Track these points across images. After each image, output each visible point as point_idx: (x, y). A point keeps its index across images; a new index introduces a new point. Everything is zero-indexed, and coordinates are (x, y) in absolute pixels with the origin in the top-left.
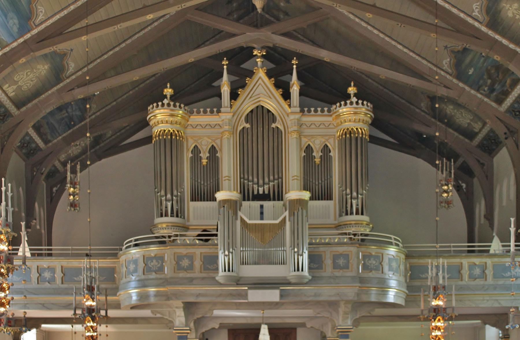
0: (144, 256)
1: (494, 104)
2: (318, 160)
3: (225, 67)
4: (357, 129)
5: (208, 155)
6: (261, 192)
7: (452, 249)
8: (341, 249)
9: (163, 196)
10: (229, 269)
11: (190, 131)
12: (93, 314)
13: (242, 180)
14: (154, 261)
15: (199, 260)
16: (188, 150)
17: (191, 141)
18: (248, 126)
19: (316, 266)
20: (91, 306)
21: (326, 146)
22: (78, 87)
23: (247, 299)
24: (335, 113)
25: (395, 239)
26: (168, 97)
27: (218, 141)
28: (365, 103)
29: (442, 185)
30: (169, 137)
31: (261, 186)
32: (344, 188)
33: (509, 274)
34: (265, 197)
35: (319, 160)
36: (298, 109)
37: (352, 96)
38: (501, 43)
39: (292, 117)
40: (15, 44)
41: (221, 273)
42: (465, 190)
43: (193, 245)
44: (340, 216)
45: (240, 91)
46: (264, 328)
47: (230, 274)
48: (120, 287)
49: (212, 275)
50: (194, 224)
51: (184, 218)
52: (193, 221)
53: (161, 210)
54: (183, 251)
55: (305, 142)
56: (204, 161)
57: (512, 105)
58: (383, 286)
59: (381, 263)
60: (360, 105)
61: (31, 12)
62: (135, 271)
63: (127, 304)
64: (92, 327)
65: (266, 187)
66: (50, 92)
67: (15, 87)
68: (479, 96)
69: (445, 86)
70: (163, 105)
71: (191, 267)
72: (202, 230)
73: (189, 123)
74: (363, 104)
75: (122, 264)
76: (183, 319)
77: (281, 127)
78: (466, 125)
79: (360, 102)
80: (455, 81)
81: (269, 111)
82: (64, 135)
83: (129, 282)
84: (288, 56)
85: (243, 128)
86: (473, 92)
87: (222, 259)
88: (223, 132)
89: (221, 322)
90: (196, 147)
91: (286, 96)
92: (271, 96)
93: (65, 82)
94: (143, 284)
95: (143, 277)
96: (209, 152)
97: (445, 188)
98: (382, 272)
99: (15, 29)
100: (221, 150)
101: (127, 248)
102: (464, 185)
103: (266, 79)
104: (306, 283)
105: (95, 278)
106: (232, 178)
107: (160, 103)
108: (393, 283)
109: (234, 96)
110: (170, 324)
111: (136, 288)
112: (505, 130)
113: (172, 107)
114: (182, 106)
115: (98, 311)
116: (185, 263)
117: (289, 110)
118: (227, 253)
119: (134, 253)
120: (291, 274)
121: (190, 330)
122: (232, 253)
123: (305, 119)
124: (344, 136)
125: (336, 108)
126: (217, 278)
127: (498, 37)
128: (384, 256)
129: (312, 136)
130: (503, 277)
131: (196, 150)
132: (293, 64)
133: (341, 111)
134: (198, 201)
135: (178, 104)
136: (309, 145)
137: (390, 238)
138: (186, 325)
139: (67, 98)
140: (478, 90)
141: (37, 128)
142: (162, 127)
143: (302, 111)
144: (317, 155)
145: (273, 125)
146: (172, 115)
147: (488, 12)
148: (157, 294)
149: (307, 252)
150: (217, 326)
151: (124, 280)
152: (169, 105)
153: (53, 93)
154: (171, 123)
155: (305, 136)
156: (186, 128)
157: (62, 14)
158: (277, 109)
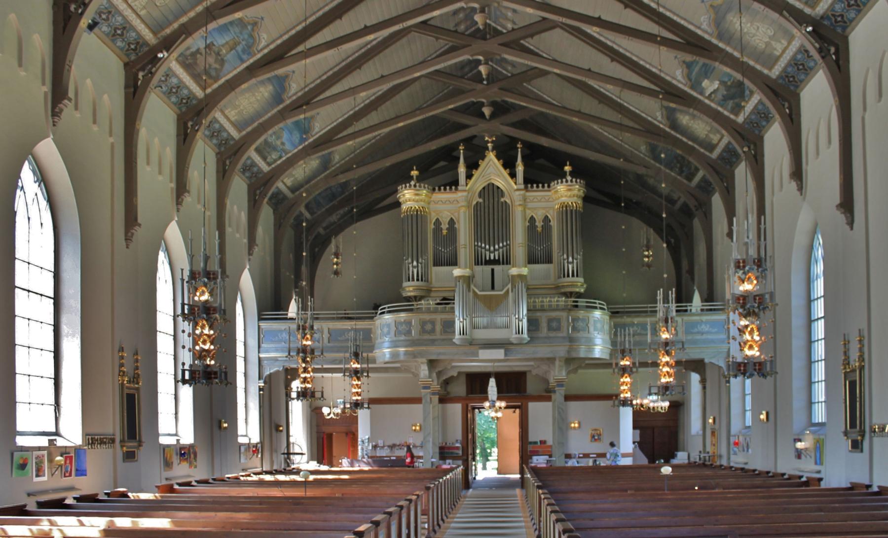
0: (395, 321)
1: (685, 181)
2: (539, 229)
3: (462, 151)
4: (572, 203)
5: (448, 226)
6: (492, 258)
7: (649, 309)
8: (554, 314)
9: (410, 263)
10: (463, 332)
11: (432, 206)
12: (359, 375)
13: (476, 247)
14: (404, 325)
15: (440, 324)
16: (431, 222)
17: (433, 214)
18: (481, 200)
19: (534, 328)
20: (356, 368)
21: (546, 217)
22: (342, 173)
23: (478, 356)
24: (554, 189)
25: (600, 304)
26: (415, 177)
27: (456, 214)
28: (578, 180)
29: (644, 251)
30: (415, 213)
31: (492, 252)
32: (561, 253)
33: (696, 330)
34: (496, 262)
35: (541, 229)
36: (522, 186)
37: (568, 174)
38: (681, 140)
39: (517, 193)
40: (296, 150)
41: (457, 336)
42: (673, 245)
43: (435, 311)
44: (559, 277)
45: (474, 172)
46: (492, 382)
47: (465, 337)
48: (376, 346)
49: (450, 337)
50: (436, 286)
51: (428, 281)
52: (435, 283)
53: (409, 274)
54: (427, 317)
55: (529, 214)
56: (445, 232)
57: (699, 183)
58: (590, 344)
59: (587, 325)
60: (574, 183)
61: (310, 128)
62: (389, 333)
63: (381, 360)
64: (357, 385)
65: (497, 253)
66: (318, 178)
67: (292, 179)
68: (673, 174)
69: (645, 167)
70: (410, 186)
71: (433, 331)
72: (442, 298)
73: (432, 199)
74: (576, 182)
75: (378, 327)
76: (427, 372)
77: (508, 201)
78: (704, 136)
79: (574, 180)
80: (652, 162)
81: (498, 188)
82: (328, 207)
83: (384, 342)
84: (514, 140)
85: (477, 203)
86: (668, 171)
87: (458, 325)
88: (459, 207)
89: (458, 371)
90: (437, 220)
91: (513, 175)
92: (500, 175)
93: (331, 170)
94: (394, 344)
95: (395, 339)
96: (449, 224)
97: (646, 253)
98: (589, 332)
99: (297, 141)
100: (458, 222)
101: (381, 313)
102: (673, 241)
103: (496, 160)
104: (526, 343)
105: (359, 345)
106: (468, 247)
107: (408, 185)
108: (598, 341)
109: (469, 176)
110: (416, 375)
111: (388, 348)
112: (696, 203)
113: (418, 188)
114: (426, 186)
115: (362, 373)
116: (428, 327)
117: (515, 187)
118: (461, 320)
119: (388, 319)
120: (514, 337)
121: (432, 381)
122: (466, 320)
123: (528, 194)
124: (561, 209)
125: (554, 185)
126: (454, 340)
127: (678, 136)
128: (590, 318)
129: (535, 209)
130: (692, 333)
131: (438, 223)
132: (518, 148)
133: (559, 187)
134: (439, 266)
135: (422, 185)
136: (532, 216)
137: (595, 303)
138: (430, 377)
139: (333, 183)
140: (671, 169)
141: (307, 207)
142: (409, 204)
143: (526, 188)
144: (539, 224)
145: (502, 200)
146: (417, 195)
147: (668, 118)
148: (406, 353)
149: (526, 318)
150: (455, 374)
151: (379, 341)
152: (415, 186)
153: (321, 179)
154: (417, 201)
155: (529, 209)
156: (429, 203)
157: (332, 125)
158: (506, 186)
